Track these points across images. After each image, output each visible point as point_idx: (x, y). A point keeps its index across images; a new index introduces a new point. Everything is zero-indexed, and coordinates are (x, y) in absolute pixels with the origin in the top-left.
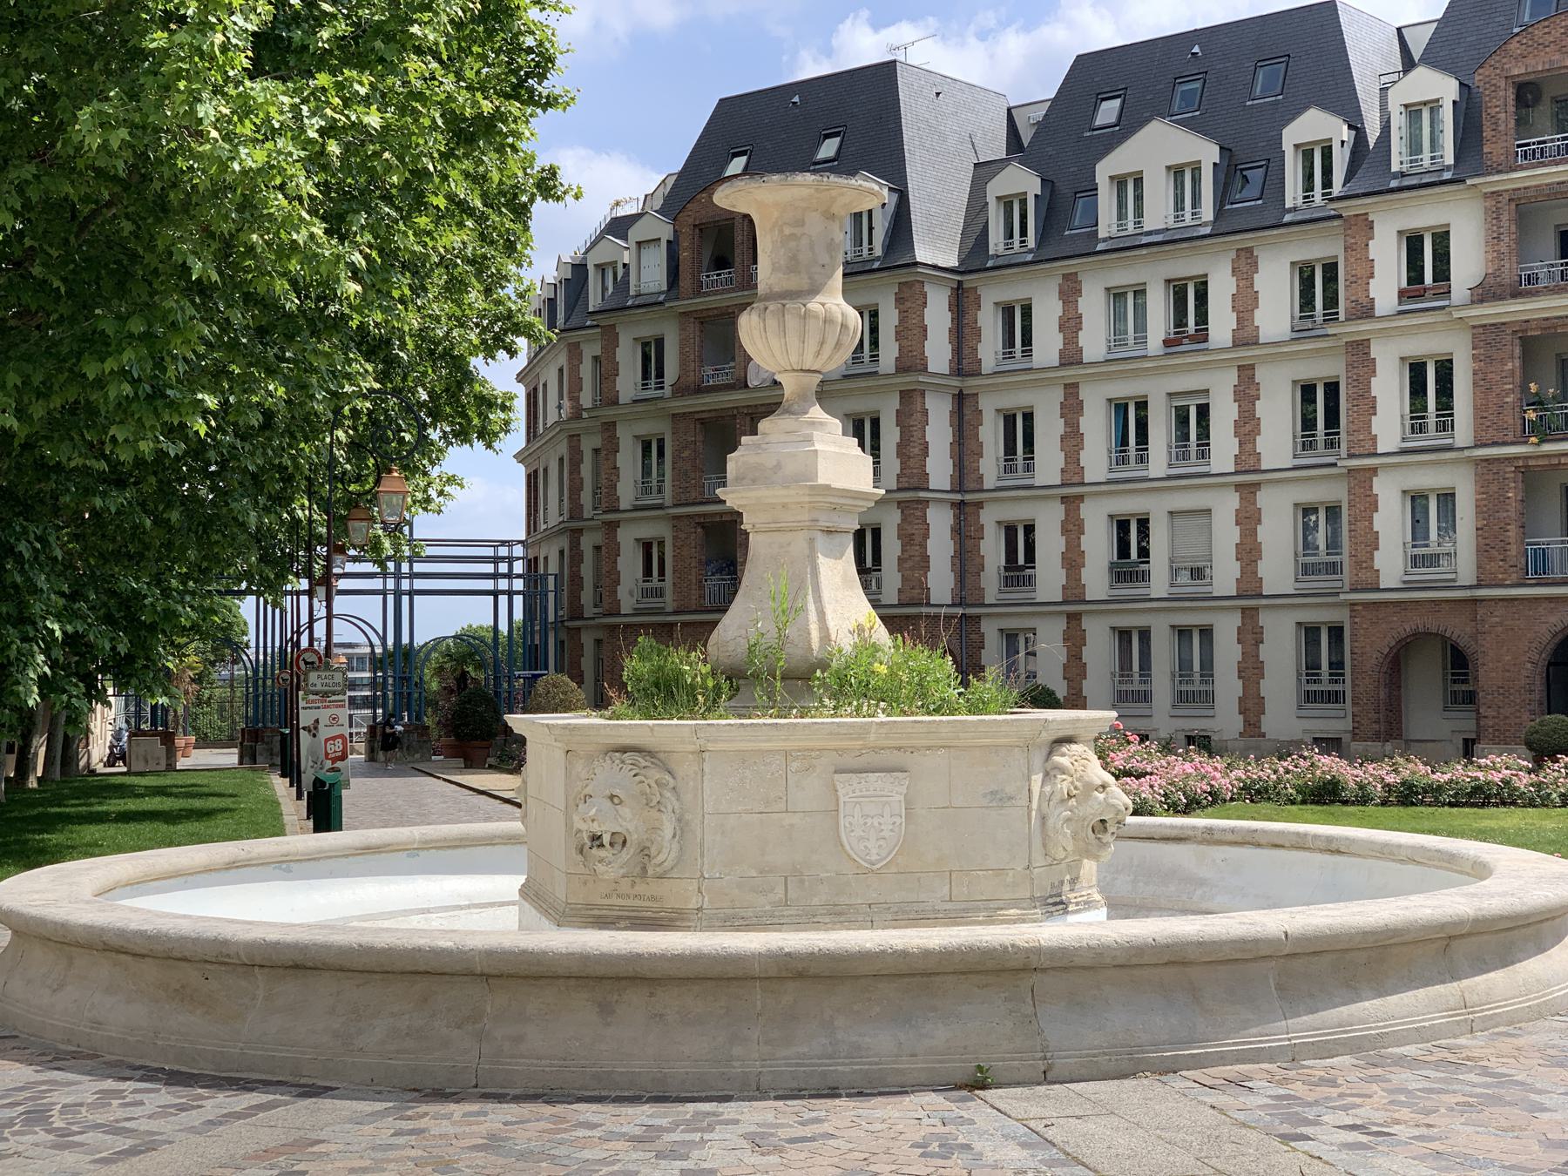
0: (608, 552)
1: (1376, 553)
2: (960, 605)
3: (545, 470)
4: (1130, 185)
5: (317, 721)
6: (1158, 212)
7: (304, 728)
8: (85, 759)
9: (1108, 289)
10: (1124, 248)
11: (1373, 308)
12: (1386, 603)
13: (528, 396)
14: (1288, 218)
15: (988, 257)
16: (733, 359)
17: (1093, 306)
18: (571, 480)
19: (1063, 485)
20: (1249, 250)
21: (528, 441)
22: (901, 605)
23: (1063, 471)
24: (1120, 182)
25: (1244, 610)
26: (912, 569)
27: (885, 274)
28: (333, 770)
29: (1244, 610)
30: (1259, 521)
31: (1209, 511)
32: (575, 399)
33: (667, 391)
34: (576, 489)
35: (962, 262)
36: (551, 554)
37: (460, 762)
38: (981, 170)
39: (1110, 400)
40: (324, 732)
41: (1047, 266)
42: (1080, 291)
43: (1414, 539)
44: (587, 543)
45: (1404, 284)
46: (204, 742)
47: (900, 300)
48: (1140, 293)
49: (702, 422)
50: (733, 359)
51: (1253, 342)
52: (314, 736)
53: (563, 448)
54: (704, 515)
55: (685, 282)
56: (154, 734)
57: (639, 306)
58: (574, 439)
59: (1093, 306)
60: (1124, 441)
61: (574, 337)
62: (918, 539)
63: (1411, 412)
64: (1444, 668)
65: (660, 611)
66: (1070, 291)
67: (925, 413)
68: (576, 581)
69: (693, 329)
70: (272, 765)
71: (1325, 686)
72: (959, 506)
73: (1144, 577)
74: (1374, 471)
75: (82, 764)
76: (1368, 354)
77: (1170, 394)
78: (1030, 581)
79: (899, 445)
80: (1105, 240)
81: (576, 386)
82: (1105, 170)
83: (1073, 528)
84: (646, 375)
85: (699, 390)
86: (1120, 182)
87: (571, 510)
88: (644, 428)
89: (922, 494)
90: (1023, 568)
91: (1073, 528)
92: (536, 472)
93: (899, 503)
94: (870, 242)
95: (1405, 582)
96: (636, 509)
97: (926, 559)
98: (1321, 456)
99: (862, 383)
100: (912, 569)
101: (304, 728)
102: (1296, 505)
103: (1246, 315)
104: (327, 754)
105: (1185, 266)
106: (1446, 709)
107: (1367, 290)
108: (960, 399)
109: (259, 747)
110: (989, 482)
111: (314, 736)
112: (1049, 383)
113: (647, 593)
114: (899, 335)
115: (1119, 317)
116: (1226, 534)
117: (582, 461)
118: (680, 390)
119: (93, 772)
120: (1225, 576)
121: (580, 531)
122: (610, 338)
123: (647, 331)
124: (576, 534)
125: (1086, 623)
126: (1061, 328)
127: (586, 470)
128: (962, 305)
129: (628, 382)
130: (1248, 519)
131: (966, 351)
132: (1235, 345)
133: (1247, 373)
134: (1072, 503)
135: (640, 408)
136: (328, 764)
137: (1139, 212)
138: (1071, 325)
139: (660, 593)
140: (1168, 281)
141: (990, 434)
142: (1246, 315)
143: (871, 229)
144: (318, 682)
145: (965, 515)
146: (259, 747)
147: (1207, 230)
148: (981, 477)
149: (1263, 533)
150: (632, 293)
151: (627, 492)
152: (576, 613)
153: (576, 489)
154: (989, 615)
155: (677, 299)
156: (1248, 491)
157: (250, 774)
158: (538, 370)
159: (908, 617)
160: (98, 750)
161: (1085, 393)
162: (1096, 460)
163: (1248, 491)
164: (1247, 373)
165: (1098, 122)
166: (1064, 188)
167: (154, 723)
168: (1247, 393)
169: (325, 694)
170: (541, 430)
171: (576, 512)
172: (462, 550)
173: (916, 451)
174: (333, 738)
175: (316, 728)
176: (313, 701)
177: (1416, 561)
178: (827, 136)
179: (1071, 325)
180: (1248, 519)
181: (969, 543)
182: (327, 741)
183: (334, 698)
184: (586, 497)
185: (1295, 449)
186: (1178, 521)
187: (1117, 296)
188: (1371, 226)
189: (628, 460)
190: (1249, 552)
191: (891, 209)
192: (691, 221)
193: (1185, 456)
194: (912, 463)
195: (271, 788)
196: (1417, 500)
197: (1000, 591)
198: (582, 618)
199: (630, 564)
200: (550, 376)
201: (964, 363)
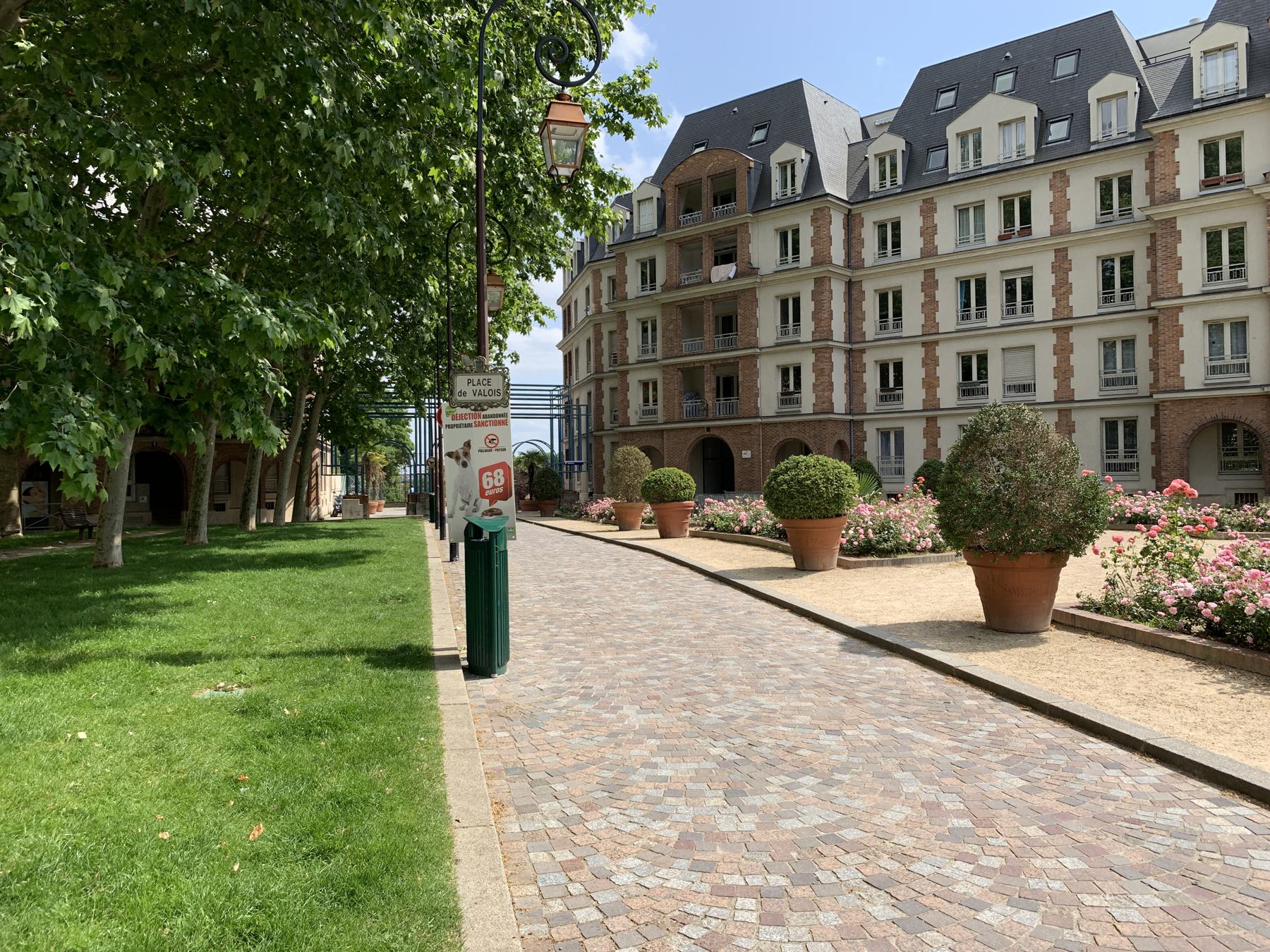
0: (620, 391)
1: (1181, 365)
2: (850, 414)
3: (577, 350)
4: (972, 139)
5: (468, 444)
6: (992, 155)
7: (450, 455)
8: (316, 511)
9: (955, 207)
10: (967, 179)
11: (1178, 195)
12: (1190, 400)
13: (564, 312)
14: (1093, 148)
15: (869, 193)
16: (701, 268)
17: (945, 218)
18: (596, 350)
19: (923, 335)
20: (1063, 172)
21: (565, 335)
22: (814, 414)
23: (923, 326)
24: (963, 137)
25: (1060, 411)
26: (823, 390)
27: (805, 203)
28: (491, 512)
29: (1060, 411)
30: (1072, 352)
31: (1033, 347)
32: (597, 302)
33: (658, 289)
34: (599, 355)
35: (850, 198)
36: (581, 397)
37: (538, 513)
38: (854, 148)
39: (957, 279)
40: (479, 460)
41: (913, 194)
42: (936, 209)
43: (1210, 355)
44: (606, 386)
45: (1203, 178)
46: (391, 503)
47: (814, 220)
48: (979, 208)
49: (681, 307)
50: (701, 268)
51: (1067, 232)
52: (465, 465)
53: (590, 333)
54: (683, 364)
55: (670, 221)
56: (356, 497)
57: (640, 239)
58: (597, 327)
59: (945, 218)
60: (967, 305)
61: (596, 266)
62: (827, 372)
63: (1230, 263)
64: (1218, 446)
65: (655, 423)
66: (928, 210)
67: (831, 292)
68: (599, 408)
69: (675, 249)
70: (425, 516)
71: (1121, 460)
72: (849, 352)
73: (985, 392)
74: (1180, 308)
75: (313, 515)
76: (1175, 227)
77: (1002, 272)
78: (899, 398)
79: (813, 313)
80: (953, 175)
81: (598, 294)
82: (952, 131)
83: (930, 362)
84: (644, 282)
85: (679, 287)
86: (963, 137)
87: (596, 368)
88: (643, 314)
89: (830, 343)
90: (892, 390)
91: (930, 362)
92: (570, 353)
93: (813, 350)
94: (793, 185)
95: (1206, 385)
96: (639, 362)
97: (831, 384)
98: (1118, 305)
99: (789, 275)
100: (823, 390)
101: (450, 455)
102: (1100, 340)
103: (1060, 215)
104: (482, 491)
105: (1014, 187)
106: (1220, 474)
107: (1174, 183)
108: (850, 284)
109: (418, 505)
110: (869, 337)
111: (465, 465)
112: (913, 270)
113: (645, 413)
114: (813, 243)
115: (963, 226)
116: (1046, 361)
117: (602, 339)
118: (667, 288)
119: (321, 520)
120: (1046, 389)
121: (601, 380)
122: (621, 260)
123: (645, 255)
124: (599, 382)
125: (940, 423)
126: (922, 234)
127: (605, 344)
128: (851, 223)
129: (633, 287)
130: (1063, 351)
131: (853, 254)
132: (1052, 235)
133: (1061, 255)
134: (930, 346)
135: (640, 301)
136: (485, 504)
137: (978, 155)
138: (929, 232)
139: (654, 412)
140: (1000, 198)
141: (870, 306)
142: (1060, 215)
143: (793, 176)
144: (469, 389)
145: (854, 357)
146: (418, 505)
147: (1032, 161)
148: (864, 333)
149: (1074, 359)
150: (635, 232)
151: (633, 353)
152: (600, 427)
153: (599, 355)
154: (940, 416)
155: (664, 232)
156: (1063, 332)
157: (410, 521)
158: (571, 293)
159: (820, 421)
160: (326, 507)
161: (939, 275)
162: (948, 315)
163: (1063, 332)
164: (1061, 255)
165: (940, 106)
166: (919, 148)
167: (356, 491)
168: (1062, 265)
169: (479, 407)
170: (573, 326)
171: (599, 369)
172: (533, 392)
173: (826, 316)
174: (492, 468)
175: (466, 454)
176: (462, 417)
177: (1213, 370)
178: (758, 129)
179: (929, 232)
180: (1063, 351)
181: (856, 376)
182: (482, 471)
183: (490, 411)
184: (605, 360)
185: (1099, 303)
186: (1009, 355)
187: (962, 211)
188: (1176, 138)
189: (633, 334)
190: (1064, 372)
191: (806, 163)
192: (673, 183)
193: (968, 317)
194: (823, 324)
195: (420, 530)
196: (1215, 328)
197: (877, 405)
198: (603, 430)
199: (635, 396)
200: (580, 295)
201: (853, 259)
